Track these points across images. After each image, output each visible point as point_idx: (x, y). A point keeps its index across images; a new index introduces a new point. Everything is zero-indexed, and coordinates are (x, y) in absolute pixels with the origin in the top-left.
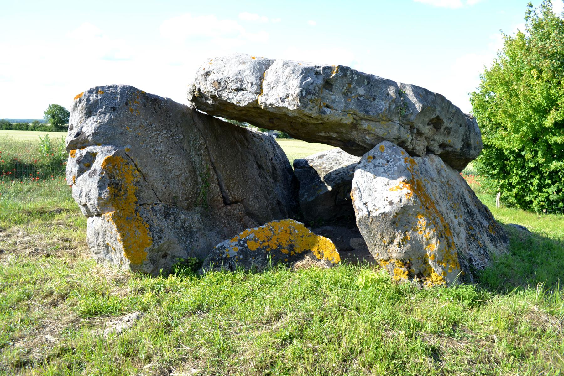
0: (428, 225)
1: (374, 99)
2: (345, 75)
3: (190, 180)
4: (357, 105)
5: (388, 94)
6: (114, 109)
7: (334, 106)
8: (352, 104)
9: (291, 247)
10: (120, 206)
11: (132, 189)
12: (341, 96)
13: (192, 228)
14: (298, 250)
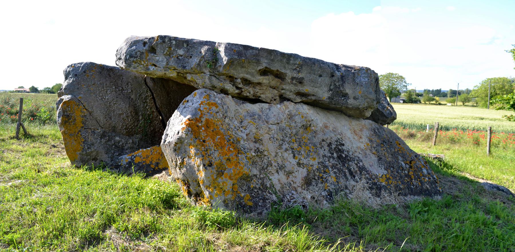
0: (196, 155)
1: (191, 57)
2: (164, 42)
3: (130, 117)
4: (176, 62)
5: (201, 52)
6: (76, 75)
7: (157, 64)
8: (171, 62)
9: (157, 164)
10: (69, 128)
11: (79, 119)
12: (164, 57)
13: (124, 146)
14: (160, 167)
